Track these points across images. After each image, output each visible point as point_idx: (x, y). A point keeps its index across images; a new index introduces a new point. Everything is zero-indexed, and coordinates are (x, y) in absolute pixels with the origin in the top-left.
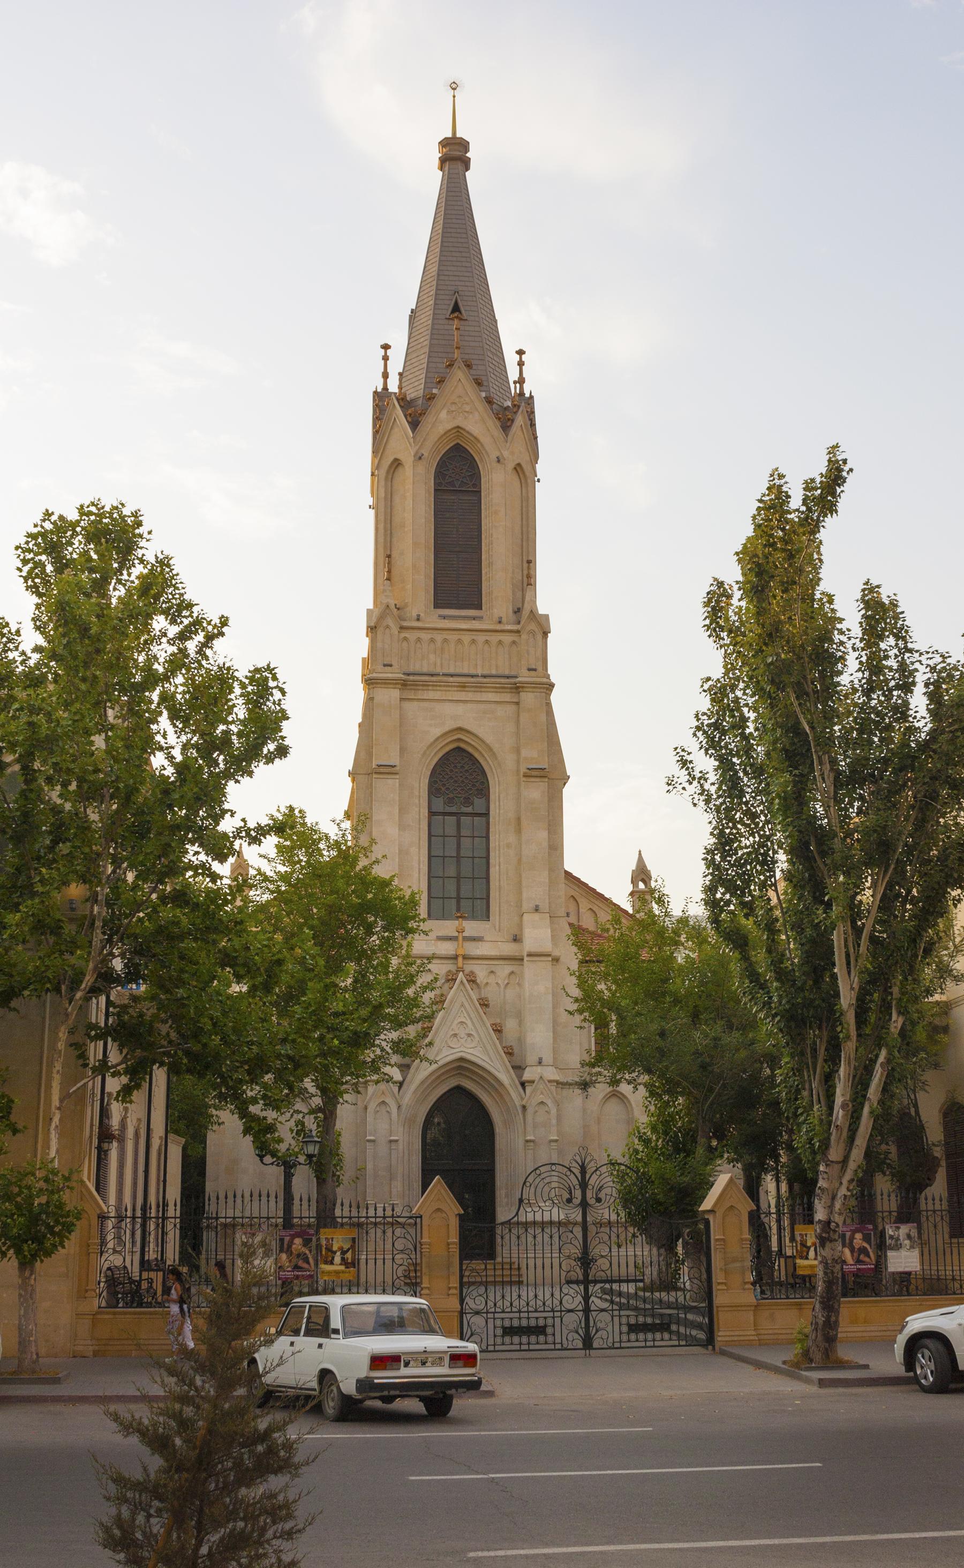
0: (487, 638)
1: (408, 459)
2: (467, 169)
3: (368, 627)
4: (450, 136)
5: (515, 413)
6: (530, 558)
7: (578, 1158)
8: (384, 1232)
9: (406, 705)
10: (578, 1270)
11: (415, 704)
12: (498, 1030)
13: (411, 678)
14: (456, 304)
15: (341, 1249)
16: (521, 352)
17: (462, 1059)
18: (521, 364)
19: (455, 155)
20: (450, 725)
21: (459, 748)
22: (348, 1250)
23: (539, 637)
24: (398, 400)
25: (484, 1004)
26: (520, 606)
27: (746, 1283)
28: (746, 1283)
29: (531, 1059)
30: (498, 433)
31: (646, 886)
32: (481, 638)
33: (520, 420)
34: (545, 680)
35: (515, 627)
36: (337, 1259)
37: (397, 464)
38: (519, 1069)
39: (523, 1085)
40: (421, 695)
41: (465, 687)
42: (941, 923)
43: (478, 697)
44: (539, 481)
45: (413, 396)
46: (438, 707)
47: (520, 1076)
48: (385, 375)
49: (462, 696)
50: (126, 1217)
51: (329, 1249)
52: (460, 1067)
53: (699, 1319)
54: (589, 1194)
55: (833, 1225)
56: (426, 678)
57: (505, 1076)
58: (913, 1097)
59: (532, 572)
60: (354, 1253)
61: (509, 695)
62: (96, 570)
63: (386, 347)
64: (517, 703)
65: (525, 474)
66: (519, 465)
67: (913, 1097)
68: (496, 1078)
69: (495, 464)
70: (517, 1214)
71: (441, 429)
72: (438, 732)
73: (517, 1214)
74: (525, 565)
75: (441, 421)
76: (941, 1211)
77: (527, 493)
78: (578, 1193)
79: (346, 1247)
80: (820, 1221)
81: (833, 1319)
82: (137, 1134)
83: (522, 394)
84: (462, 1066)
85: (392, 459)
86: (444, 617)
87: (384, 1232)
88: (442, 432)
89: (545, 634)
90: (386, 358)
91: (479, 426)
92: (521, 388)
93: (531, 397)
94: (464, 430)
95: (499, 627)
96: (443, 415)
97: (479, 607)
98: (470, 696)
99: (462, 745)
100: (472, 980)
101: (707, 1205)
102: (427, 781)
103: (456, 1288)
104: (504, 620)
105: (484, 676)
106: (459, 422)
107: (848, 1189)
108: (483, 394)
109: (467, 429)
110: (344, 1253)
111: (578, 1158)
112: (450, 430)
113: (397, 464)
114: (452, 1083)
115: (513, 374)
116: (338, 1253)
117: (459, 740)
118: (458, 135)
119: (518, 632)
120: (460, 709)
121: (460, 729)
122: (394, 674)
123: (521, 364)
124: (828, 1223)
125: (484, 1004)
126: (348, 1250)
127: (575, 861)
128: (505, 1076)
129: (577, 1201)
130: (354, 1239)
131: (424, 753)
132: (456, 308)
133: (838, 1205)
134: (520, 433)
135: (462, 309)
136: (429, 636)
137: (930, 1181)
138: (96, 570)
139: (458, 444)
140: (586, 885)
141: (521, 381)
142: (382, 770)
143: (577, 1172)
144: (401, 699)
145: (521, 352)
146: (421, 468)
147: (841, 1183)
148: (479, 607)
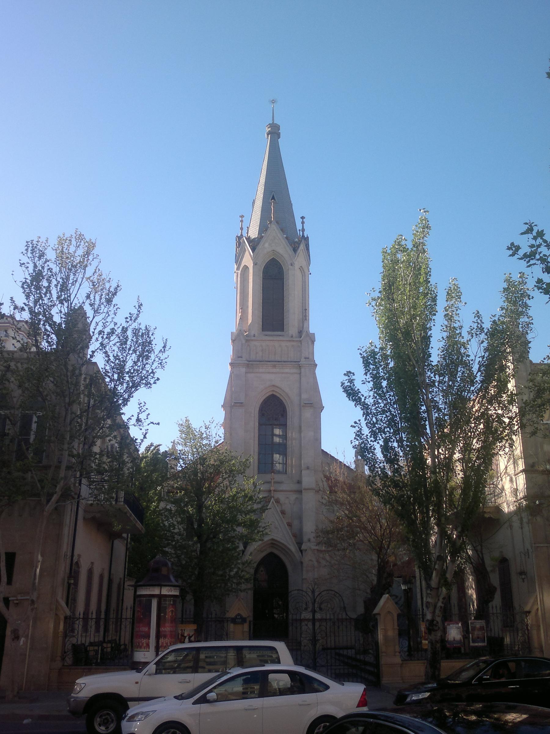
2: (279, 138)
5: (298, 243)
7: (310, 587)
10: (310, 645)
12: (289, 525)
13: (251, 363)
14: (273, 196)
15: (189, 635)
16: (303, 218)
17: (273, 539)
18: (303, 223)
19: (274, 132)
23: (310, 343)
24: (246, 238)
25: (283, 512)
26: (301, 329)
29: (305, 539)
30: (291, 252)
33: (302, 247)
34: (312, 363)
35: (298, 339)
38: (299, 544)
39: (301, 551)
42: (494, 467)
45: (253, 237)
48: (242, 229)
50: (80, 618)
52: (272, 543)
53: (372, 669)
54: (316, 606)
55: (435, 622)
56: (258, 363)
57: (293, 548)
58: (481, 555)
59: (307, 315)
63: (242, 216)
64: (300, 373)
65: (305, 273)
67: (481, 555)
68: (289, 549)
69: (290, 267)
74: (304, 311)
75: (266, 247)
76: (497, 613)
78: (310, 606)
79: (191, 634)
80: (428, 620)
81: (437, 673)
82: (101, 577)
83: (303, 236)
84: (274, 543)
86: (266, 335)
89: (313, 342)
90: (242, 221)
91: (283, 250)
92: (303, 234)
93: (308, 237)
96: (267, 245)
97: (282, 330)
99: (274, 393)
100: (278, 501)
101: (376, 611)
105: (284, 362)
107: (442, 603)
108: (285, 236)
111: (310, 587)
114: (271, 393)
115: (299, 226)
116: (187, 637)
117: (273, 391)
121: (274, 386)
123: (303, 223)
124: (433, 620)
125: (283, 512)
127: (326, 446)
128: (293, 548)
129: (310, 610)
132: (273, 198)
133: (437, 612)
135: (276, 198)
137: (492, 598)
141: (303, 230)
142: (236, 405)
143: (310, 594)
145: (303, 218)
147: (439, 600)
148: (282, 330)
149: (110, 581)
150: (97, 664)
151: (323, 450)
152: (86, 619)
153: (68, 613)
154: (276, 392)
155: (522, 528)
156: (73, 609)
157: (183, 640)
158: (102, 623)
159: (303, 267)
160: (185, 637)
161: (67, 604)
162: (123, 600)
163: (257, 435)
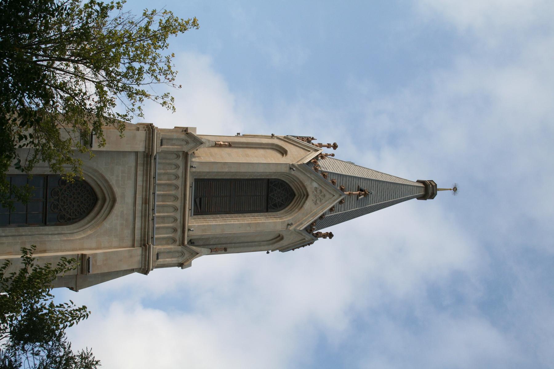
0: (179, 220)
3: (187, 128)
4: (438, 187)
6: (228, 250)
9: (132, 158)
11: (133, 164)
20: (117, 191)
21: (96, 199)
32: (178, 215)
37: (283, 152)
40: (140, 168)
41: (146, 203)
43: (138, 214)
44: (268, 253)
46: (131, 183)
49: (139, 201)
61: (139, 239)
63: (335, 146)
66: (282, 238)
71: (307, 183)
72: (113, 182)
74: (224, 246)
77: (264, 245)
85: (286, 148)
88: (305, 184)
94: (306, 199)
96: (315, 185)
98: (139, 207)
99: (99, 203)
104: (191, 232)
106: (311, 197)
109: (307, 202)
112: (306, 189)
113: (283, 152)
114: (100, 195)
115: (323, 231)
118: (438, 192)
119: (183, 244)
120: (129, 200)
121: (114, 201)
122: (157, 148)
131: (96, 171)
134: (301, 239)
136: (180, 175)
139: (295, 195)
144: (136, 153)
146: (285, 170)
159: (281, 242)
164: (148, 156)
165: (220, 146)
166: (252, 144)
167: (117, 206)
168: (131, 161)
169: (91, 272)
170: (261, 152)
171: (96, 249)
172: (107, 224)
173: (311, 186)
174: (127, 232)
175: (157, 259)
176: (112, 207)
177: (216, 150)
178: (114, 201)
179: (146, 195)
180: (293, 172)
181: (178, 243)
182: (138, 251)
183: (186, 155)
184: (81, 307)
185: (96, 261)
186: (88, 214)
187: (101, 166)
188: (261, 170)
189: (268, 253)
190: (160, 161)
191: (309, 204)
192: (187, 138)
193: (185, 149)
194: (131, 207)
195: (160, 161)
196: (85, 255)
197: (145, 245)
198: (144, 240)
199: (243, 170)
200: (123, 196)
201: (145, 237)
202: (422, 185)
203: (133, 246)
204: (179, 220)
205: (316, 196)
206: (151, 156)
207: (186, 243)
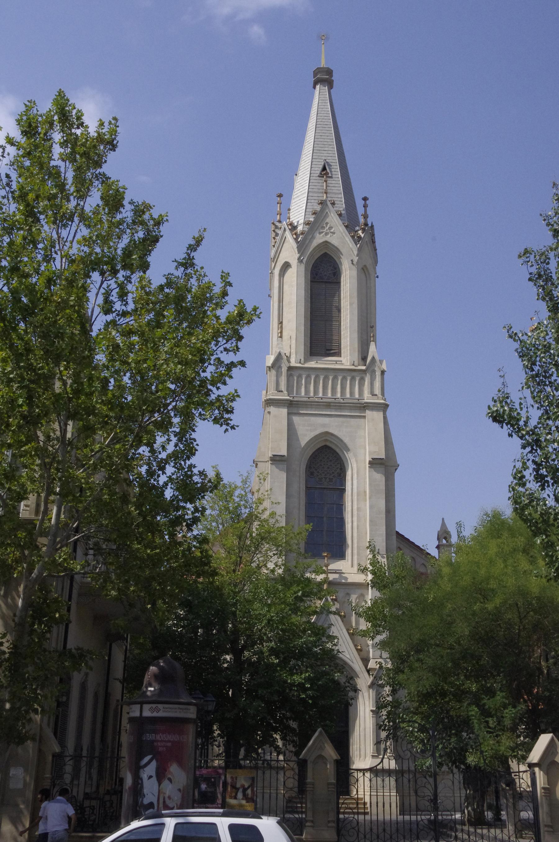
1: (294, 263)
8: (383, 780)
16: (365, 199)
18: (365, 206)
22: (249, 787)
27: (329, 822)
28: (329, 822)
31: (447, 542)
36: (240, 795)
37: (286, 266)
44: (377, 277)
47: (366, 666)
51: (234, 787)
60: (252, 790)
62: (63, 154)
66: (365, 266)
70: (382, 761)
73: (382, 761)
82: (96, 695)
87: (383, 780)
93: (372, 226)
95: (353, 367)
99: (328, 444)
102: (311, 453)
103: (334, 822)
104: (356, 363)
106: (328, 238)
110: (245, 790)
114: (323, 444)
116: (241, 790)
117: (326, 440)
120: (326, 420)
122: (285, 396)
123: (365, 206)
126: (249, 787)
130: (253, 779)
138: (63, 154)
140: (408, 540)
141: (366, 216)
144: (289, 414)
145: (365, 199)
146: (303, 267)
149: (107, 704)
150: (335, 268)
151: (397, 533)
152: (77, 757)
153: (57, 749)
154: (331, 442)
155: (263, 793)
156: (62, 743)
157: (234, 794)
158: (96, 764)
159: (368, 266)
160: (238, 789)
161: (55, 734)
162: (281, 323)
163: (303, 502)
164: (293, 406)
165: (281, 332)
166: (318, 388)
167: (331, 431)
168: (296, 419)
169: (383, 457)
170: (286, 287)
171: (365, 449)
172: (346, 440)
173: (319, 239)
174: (353, 421)
175: (376, 395)
176: (332, 435)
177: (285, 334)
178: (327, 433)
179: (323, 405)
180: (305, 259)
181: (364, 375)
182: (368, 413)
183: (290, 368)
184: (193, 242)
185: (375, 452)
186: (335, 451)
187: (303, 441)
188: (303, 292)
189: (377, 277)
190: (340, 196)
191: (334, 240)
192: (276, 368)
193: (284, 369)
194: (332, 419)
195: (340, 196)
196: (370, 461)
197: (364, 407)
198: (360, 407)
199: (303, 310)
200: (324, 425)
201: (357, 407)
202: (318, 87)
203: (364, 417)
204: (345, 374)
205: (327, 234)
206: (291, 401)
207: (364, 368)
